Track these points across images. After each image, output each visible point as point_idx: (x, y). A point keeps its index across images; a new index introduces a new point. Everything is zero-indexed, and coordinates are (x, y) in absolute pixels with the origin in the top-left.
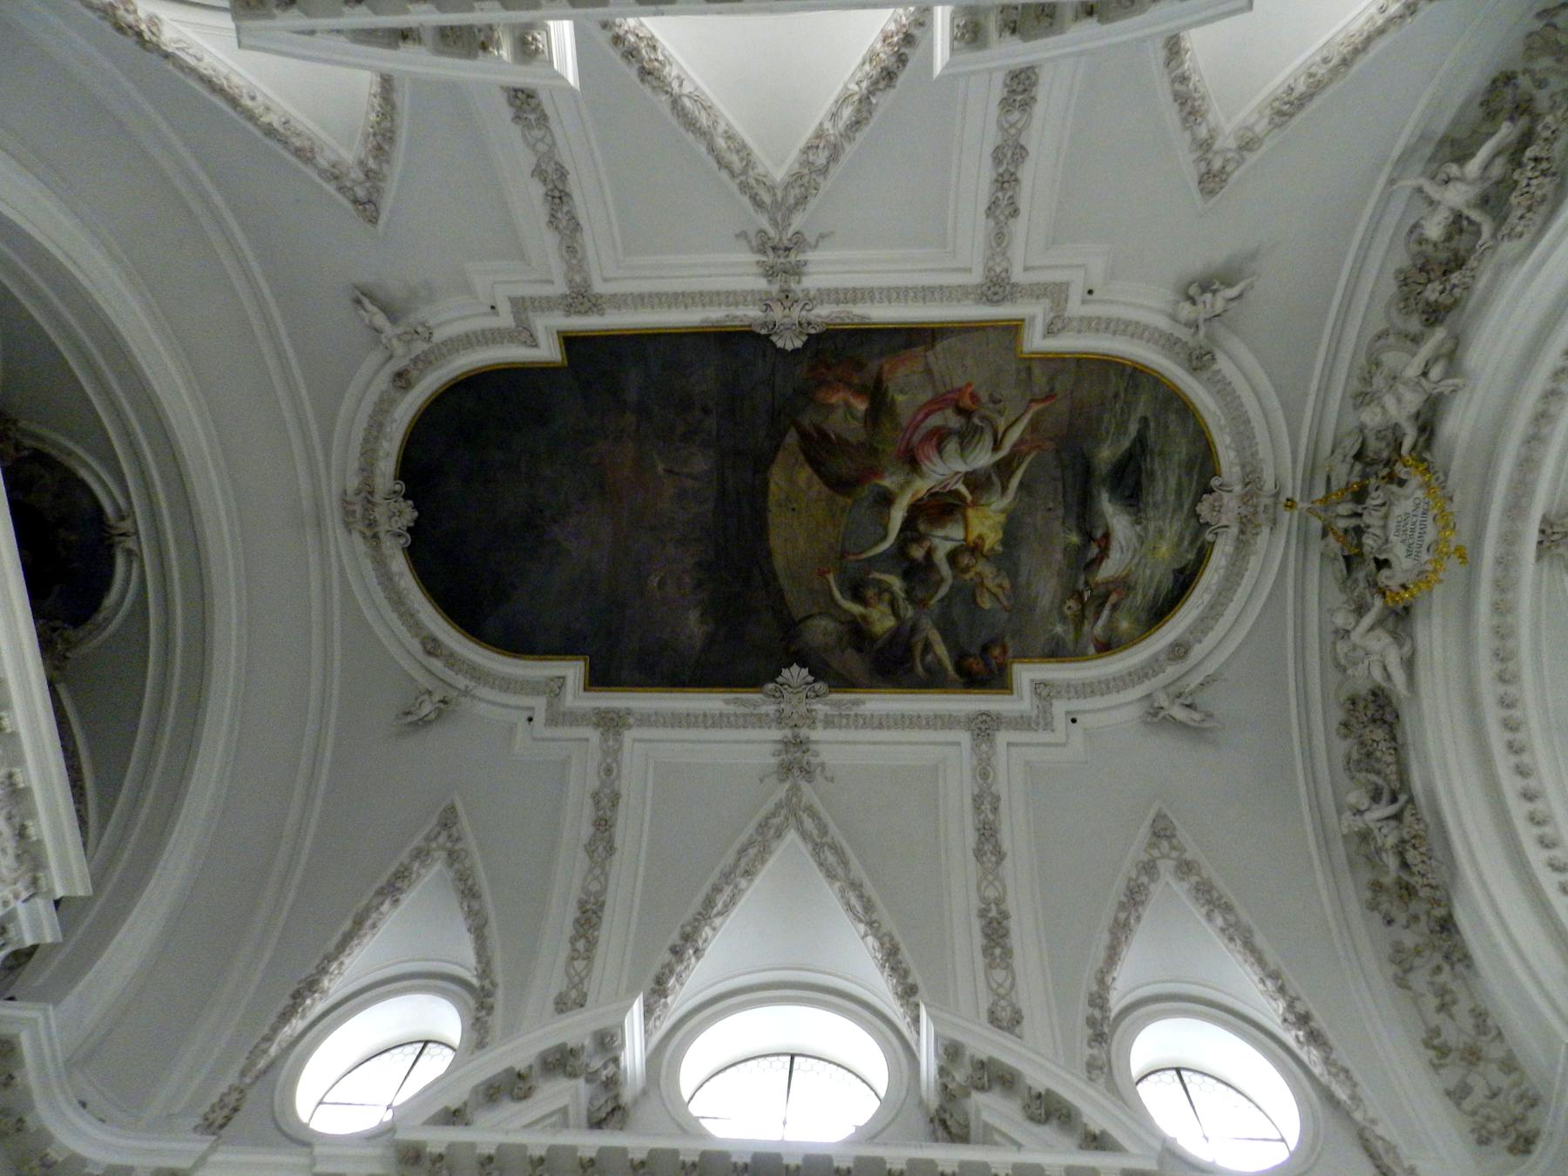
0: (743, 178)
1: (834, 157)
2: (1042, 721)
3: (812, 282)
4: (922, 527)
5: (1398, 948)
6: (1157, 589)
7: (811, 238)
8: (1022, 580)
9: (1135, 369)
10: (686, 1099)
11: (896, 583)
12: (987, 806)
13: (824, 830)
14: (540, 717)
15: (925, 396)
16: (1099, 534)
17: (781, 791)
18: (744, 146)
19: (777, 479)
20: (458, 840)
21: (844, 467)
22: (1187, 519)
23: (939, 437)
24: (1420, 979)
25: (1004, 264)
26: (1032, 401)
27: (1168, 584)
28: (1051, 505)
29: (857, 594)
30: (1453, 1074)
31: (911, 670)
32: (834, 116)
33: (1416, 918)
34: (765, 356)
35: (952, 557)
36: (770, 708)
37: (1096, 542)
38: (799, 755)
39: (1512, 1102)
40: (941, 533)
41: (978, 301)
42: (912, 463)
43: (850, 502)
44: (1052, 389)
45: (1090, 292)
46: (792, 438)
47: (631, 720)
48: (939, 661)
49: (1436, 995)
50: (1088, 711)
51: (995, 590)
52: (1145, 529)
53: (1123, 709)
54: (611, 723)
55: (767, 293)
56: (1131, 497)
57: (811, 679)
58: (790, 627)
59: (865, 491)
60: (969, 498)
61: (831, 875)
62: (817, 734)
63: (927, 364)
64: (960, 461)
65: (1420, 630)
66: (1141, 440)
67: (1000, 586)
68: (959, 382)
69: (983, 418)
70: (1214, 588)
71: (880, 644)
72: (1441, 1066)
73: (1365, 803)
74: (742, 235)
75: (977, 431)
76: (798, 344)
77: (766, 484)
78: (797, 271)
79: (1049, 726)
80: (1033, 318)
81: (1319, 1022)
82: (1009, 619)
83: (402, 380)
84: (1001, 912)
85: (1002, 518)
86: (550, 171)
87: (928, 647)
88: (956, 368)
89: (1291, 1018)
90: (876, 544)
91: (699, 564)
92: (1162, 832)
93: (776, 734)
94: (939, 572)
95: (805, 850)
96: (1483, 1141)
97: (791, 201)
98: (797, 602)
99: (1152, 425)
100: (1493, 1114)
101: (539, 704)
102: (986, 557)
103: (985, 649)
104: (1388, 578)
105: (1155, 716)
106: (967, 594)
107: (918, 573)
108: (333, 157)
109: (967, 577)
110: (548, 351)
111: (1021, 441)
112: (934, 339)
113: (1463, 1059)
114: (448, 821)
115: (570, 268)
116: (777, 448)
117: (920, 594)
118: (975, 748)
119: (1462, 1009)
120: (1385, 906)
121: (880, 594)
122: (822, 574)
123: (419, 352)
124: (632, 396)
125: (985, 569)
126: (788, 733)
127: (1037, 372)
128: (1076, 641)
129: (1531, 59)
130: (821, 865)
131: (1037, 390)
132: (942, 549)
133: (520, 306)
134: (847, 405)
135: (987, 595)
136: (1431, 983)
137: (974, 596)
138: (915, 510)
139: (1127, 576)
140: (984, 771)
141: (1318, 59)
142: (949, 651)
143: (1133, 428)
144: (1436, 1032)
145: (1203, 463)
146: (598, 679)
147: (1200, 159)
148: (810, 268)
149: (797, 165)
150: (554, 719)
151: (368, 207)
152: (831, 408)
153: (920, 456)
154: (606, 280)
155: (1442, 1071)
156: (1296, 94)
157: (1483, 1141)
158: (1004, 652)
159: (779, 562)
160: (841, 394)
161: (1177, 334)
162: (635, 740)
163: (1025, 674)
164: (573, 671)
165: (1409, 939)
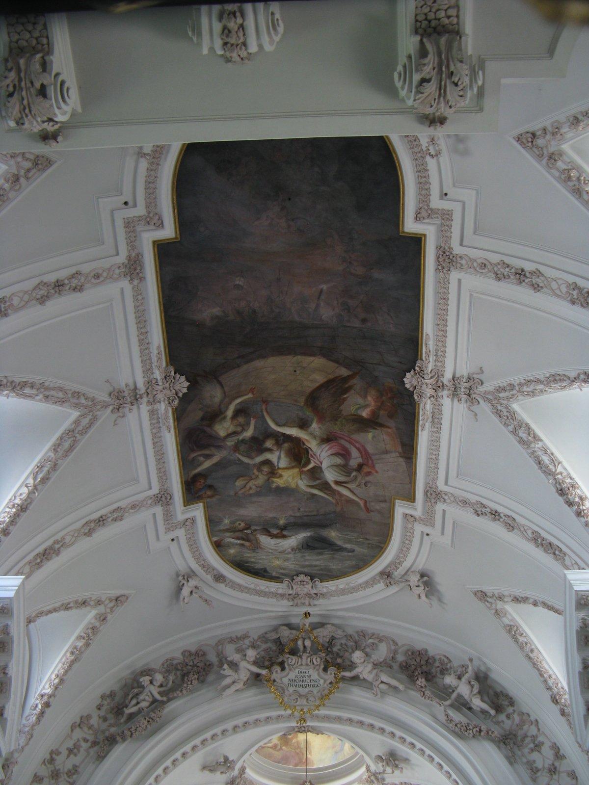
1: (522, 442)
3: (446, 402)
4: (286, 445)
5: (89, 717)
6: (254, 563)
7: (475, 408)
8: (254, 499)
11: (249, 433)
14: (131, 213)
15: (370, 449)
16: (285, 533)
17: (103, 397)
18: (534, 395)
19: (318, 362)
21: (325, 402)
22: (296, 571)
23: (344, 454)
24: (78, 734)
26: (366, 502)
27: (258, 566)
28: (302, 510)
29: (238, 412)
31: (193, 451)
35: (267, 462)
36: (158, 375)
37: (282, 532)
38: (129, 400)
40: (282, 455)
42: (327, 440)
43: (302, 404)
46: (344, 372)
47: (136, 282)
48: (199, 465)
49: (74, 745)
50: (180, 548)
51: (248, 487)
52: (289, 553)
53: (184, 560)
54: (133, 268)
55: (443, 375)
56: (308, 545)
57: (180, 395)
58: (214, 375)
59: (309, 413)
62: (144, 408)
63: (391, 452)
65: (253, 691)
66: (341, 549)
67: (251, 488)
68: (377, 466)
69: (356, 478)
71: (208, 430)
72: (45, 765)
73: (157, 684)
75: (348, 473)
76: (408, 386)
77: (312, 355)
78: (455, 394)
79: (168, 530)
84: (59, 549)
85: (293, 486)
87: (208, 457)
88: (387, 467)
90: (274, 420)
91: (254, 312)
93: (141, 385)
94: (257, 456)
95: (67, 424)
97: (499, 407)
98: (232, 378)
99: (350, 554)
101: (140, 210)
102: (268, 479)
103: (210, 487)
104: (276, 671)
105: (183, 578)
106: (245, 472)
107: (257, 445)
109: (255, 471)
110: (410, 226)
112: (406, 458)
116: (336, 361)
117: (242, 448)
119: (75, 760)
120: (105, 703)
122: (252, 391)
123: (421, 142)
124: (376, 274)
125: (261, 479)
127: (383, 505)
128: (220, 531)
129: (519, 715)
132: (273, 457)
134: (366, 406)
135: (245, 482)
136: (78, 740)
137: (242, 476)
138: (296, 442)
139: (261, 548)
141: (533, 647)
142: (205, 470)
143: (348, 546)
144: (58, 753)
145: (328, 575)
146: (163, 249)
147: (493, 595)
150: (129, 224)
152: (365, 397)
153: (332, 444)
155: (43, 766)
158: (210, 497)
159: (259, 363)
163: (198, 512)
164: (168, 232)
165: (94, 721)
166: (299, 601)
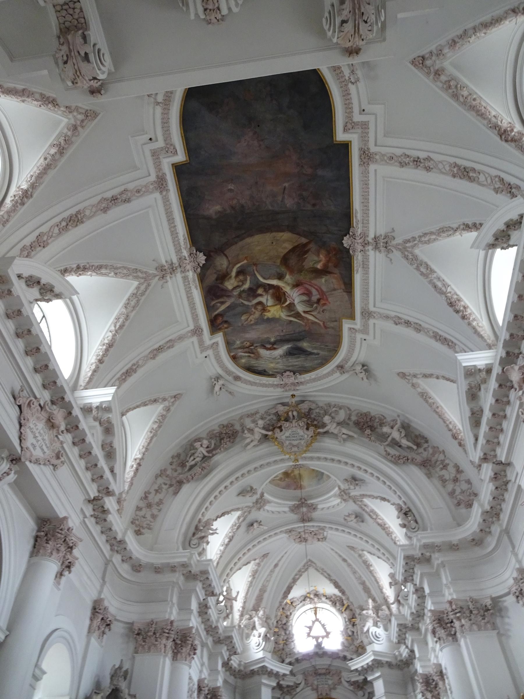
0: (418, 239)
2: (203, 347)
4: (271, 291)
7: (390, 255)
8: (254, 327)
9: (336, 351)
10: (39, 322)
11: (247, 286)
12: (168, 345)
13: (143, 294)
14: (364, 337)
15: (324, 289)
16: (275, 346)
17: (152, 271)
19: (286, 235)
20: (83, 127)
21: (293, 261)
23: (308, 294)
24: (160, 481)
25: (376, 317)
27: (260, 369)
28: (284, 331)
29: (238, 273)
30: (142, 504)
31: (213, 300)
32: (439, 279)
33: (176, 471)
34: (340, 231)
35: (260, 303)
37: (273, 346)
38: (169, 271)
39: (145, 523)
40: (269, 298)
41: (362, 308)
42: (297, 285)
43: (278, 264)
44: (328, 328)
45: (365, 340)
46: (304, 240)
47: (164, 193)
48: (218, 309)
49: (159, 487)
51: (249, 320)
52: (279, 359)
54: (367, 314)
57: (201, 265)
58: (221, 250)
59: (283, 269)
60: (284, 305)
61: (126, 306)
63: (338, 289)
64: (299, 301)
66: (311, 354)
67: (251, 320)
69: (316, 308)
70: (261, 382)
71: (221, 286)
74: (393, 230)
75: (312, 306)
78: (376, 248)
80: (356, 324)
81: (141, 468)
82: (239, 326)
83: (237, 378)
85: (277, 316)
86: (430, 164)
87: (222, 303)
88: (337, 299)
89: (138, 461)
90: (262, 276)
91: (243, 206)
92: (175, 397)
93: (175, 260)
96: (132, 523)
97: (406, 253)
98: (232, 251)
100: (139, 520)
103: (226, 322)
106: (247, 311)
107: (252, 292)
108: (449, 55)
109: (253, 309)
110: (340, 136)
111: (308, 320)
113: (147, 504)
114: (403, 375)
115: (383, 155)
116: (298, 234)
117: (244, 295)
118: (189, 332)
119: (160, 496)
120: (175, 460)
121: (241, 281)
122: (246, 258)
124: (320, 172)
125: (257, 314)
126: (177, 265)
127: (335, 323)
128: (235, 349)
130: (129, 299)
131: (328, 323)
132: (263, 299)
133: (365, 125)
134: (320, 261)
135: (247, 317)
137: (245, 313)
138: (277, 288)
140: (181, 338)
143: (315, 351)
144: (149, 493)
146: (179, 170)
148: (169, 259)
149: (420, 259)
150: (155, 154)
151: (420, 62)
152: (318, 256)
153: (300, 288)
154: (188, 326)
156: (429, 400)
157: (132, 523)
158: (226, 328)
159: (248, 240)
160: (324, 259)
161: (349, 362)
162: (374, 306)
164: (181, 157)
166: (288, 388)
